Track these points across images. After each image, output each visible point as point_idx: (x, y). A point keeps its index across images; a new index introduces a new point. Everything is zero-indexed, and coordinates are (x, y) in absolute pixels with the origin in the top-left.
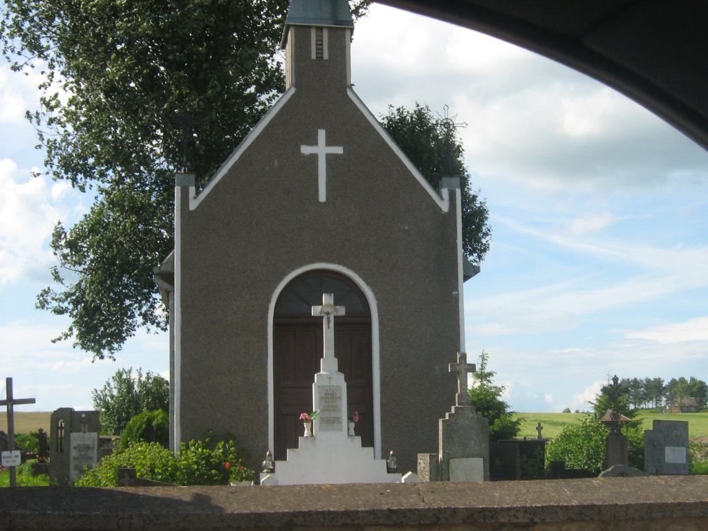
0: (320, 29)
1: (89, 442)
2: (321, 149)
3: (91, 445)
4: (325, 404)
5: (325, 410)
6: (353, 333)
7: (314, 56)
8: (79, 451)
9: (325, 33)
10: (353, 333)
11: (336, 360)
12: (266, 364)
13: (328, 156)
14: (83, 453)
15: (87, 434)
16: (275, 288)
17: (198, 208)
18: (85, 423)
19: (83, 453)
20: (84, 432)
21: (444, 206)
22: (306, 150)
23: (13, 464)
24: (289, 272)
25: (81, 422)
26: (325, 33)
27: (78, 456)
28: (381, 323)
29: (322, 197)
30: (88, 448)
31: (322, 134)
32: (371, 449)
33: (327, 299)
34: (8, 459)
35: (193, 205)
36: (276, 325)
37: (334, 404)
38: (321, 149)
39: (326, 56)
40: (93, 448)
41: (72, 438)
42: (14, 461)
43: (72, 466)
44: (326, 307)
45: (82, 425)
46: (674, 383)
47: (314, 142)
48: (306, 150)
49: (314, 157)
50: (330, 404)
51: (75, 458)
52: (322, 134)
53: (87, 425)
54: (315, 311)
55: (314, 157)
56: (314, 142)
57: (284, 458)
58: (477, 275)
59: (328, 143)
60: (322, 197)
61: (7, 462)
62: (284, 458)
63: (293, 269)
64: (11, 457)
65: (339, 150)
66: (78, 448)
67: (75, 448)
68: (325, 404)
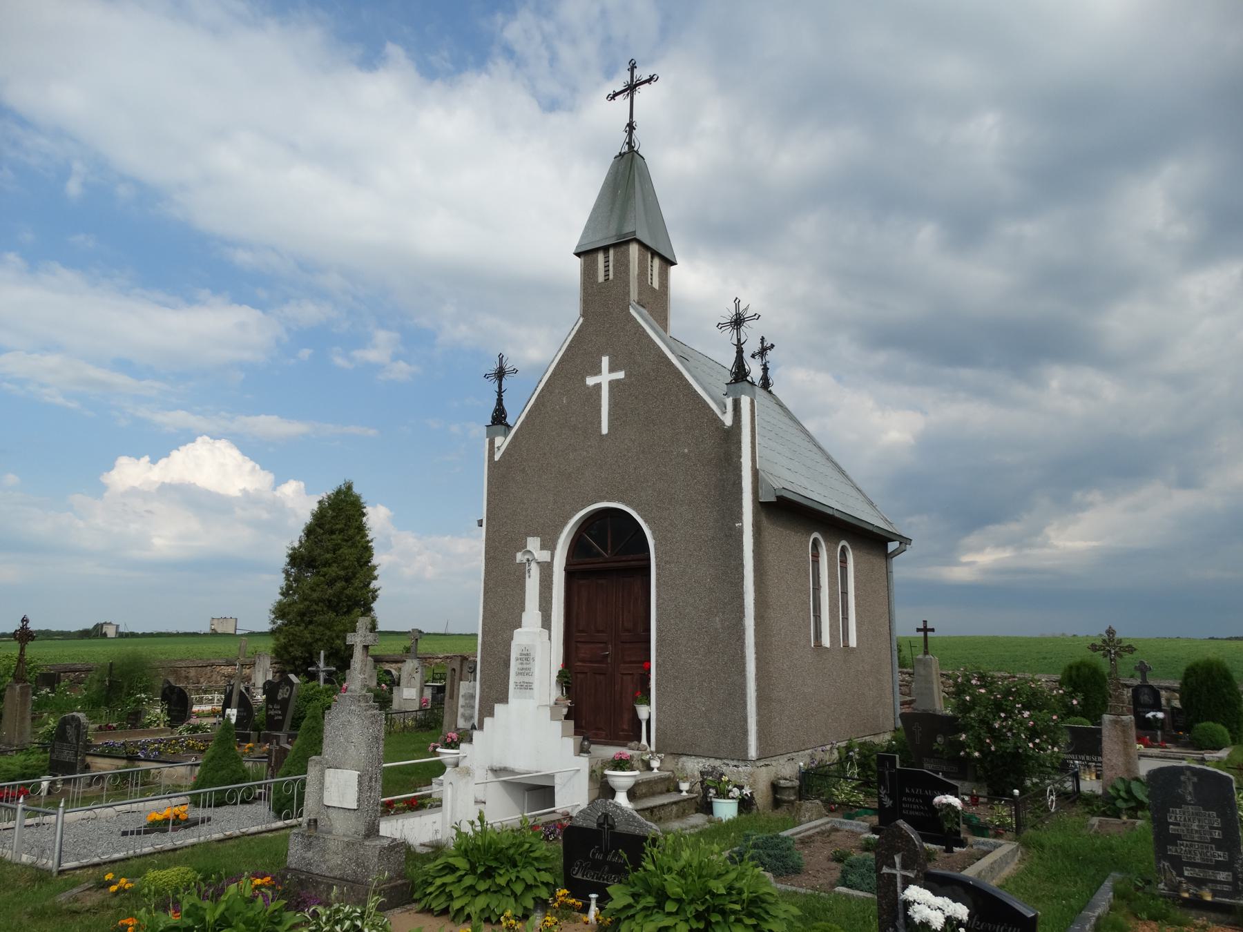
0: (605, 249)
2: (605, 378)
21: (728, 420)
29: (605, 430)
35: (497, 458)
60: (605, 430)
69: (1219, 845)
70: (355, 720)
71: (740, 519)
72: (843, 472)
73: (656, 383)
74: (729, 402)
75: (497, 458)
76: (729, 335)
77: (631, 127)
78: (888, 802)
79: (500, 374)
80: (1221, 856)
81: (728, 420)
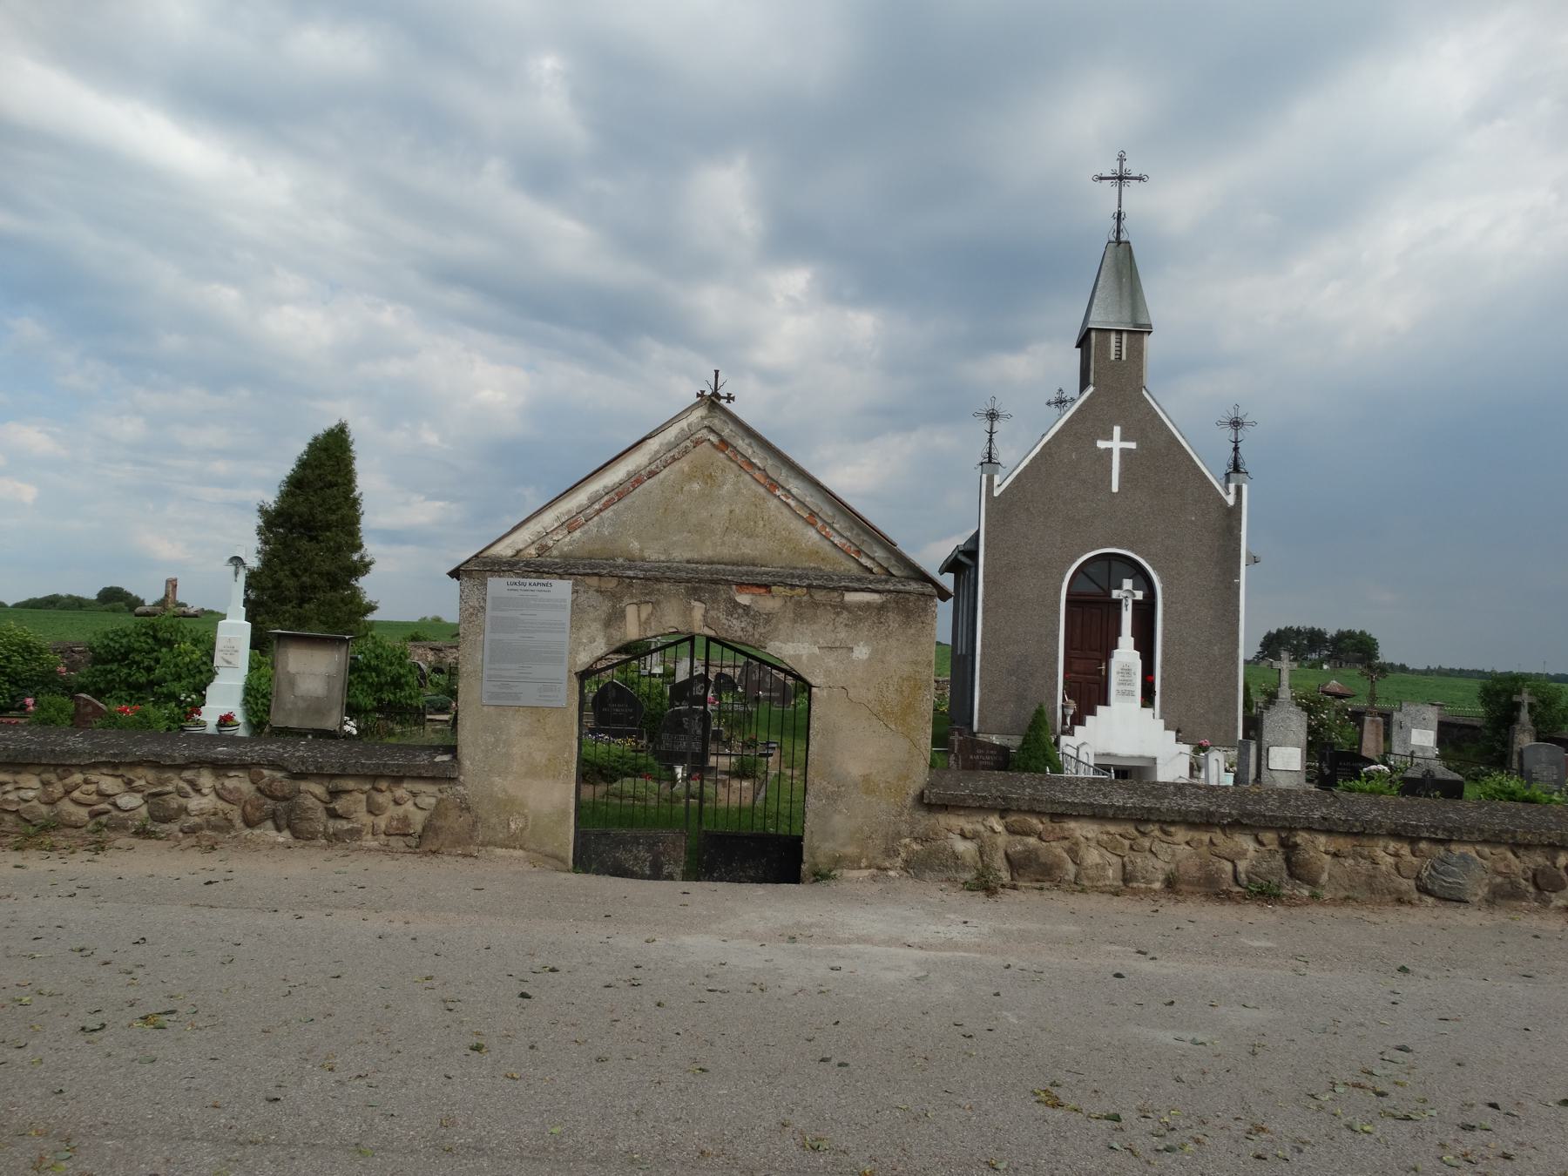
0: (1120, 332)
2: (1116, 444)
6: (1145, 612)
7: (1113, 357)
10: (1145, 612)
12: (1163, 679)
13: (1122, 450)
21: (1231, 500)
26: (1125, 336)
28: (1165, 605)
29: (1115, 489)
31: (1117, 430)
32: (1150, 711)
33: (1128, 584)
35: (996, 494)
36: (1068, 601)
38: (1116, 444)
44: (1127, 592)
46: (1342, 636)
49: (1109, 451)
52: (1117, 430)
54: (1115, 594)
55: (1109, 451)
57: (1082, 723)
59: (1111, 438)
60: (1115, 489)
62: (1082, 723)
69: (1556, 782)
70: (1294, 717)
71: (1238, 576)
72: (644, 440)
73: (1160, 454)
74: (1232, 487)
75: (996, 494)
76: (1229, 433)
77: (1119, 217)
78: (1327, 771)
79: (993, 416)
80: (1556, 787)
81: (1231, 500)
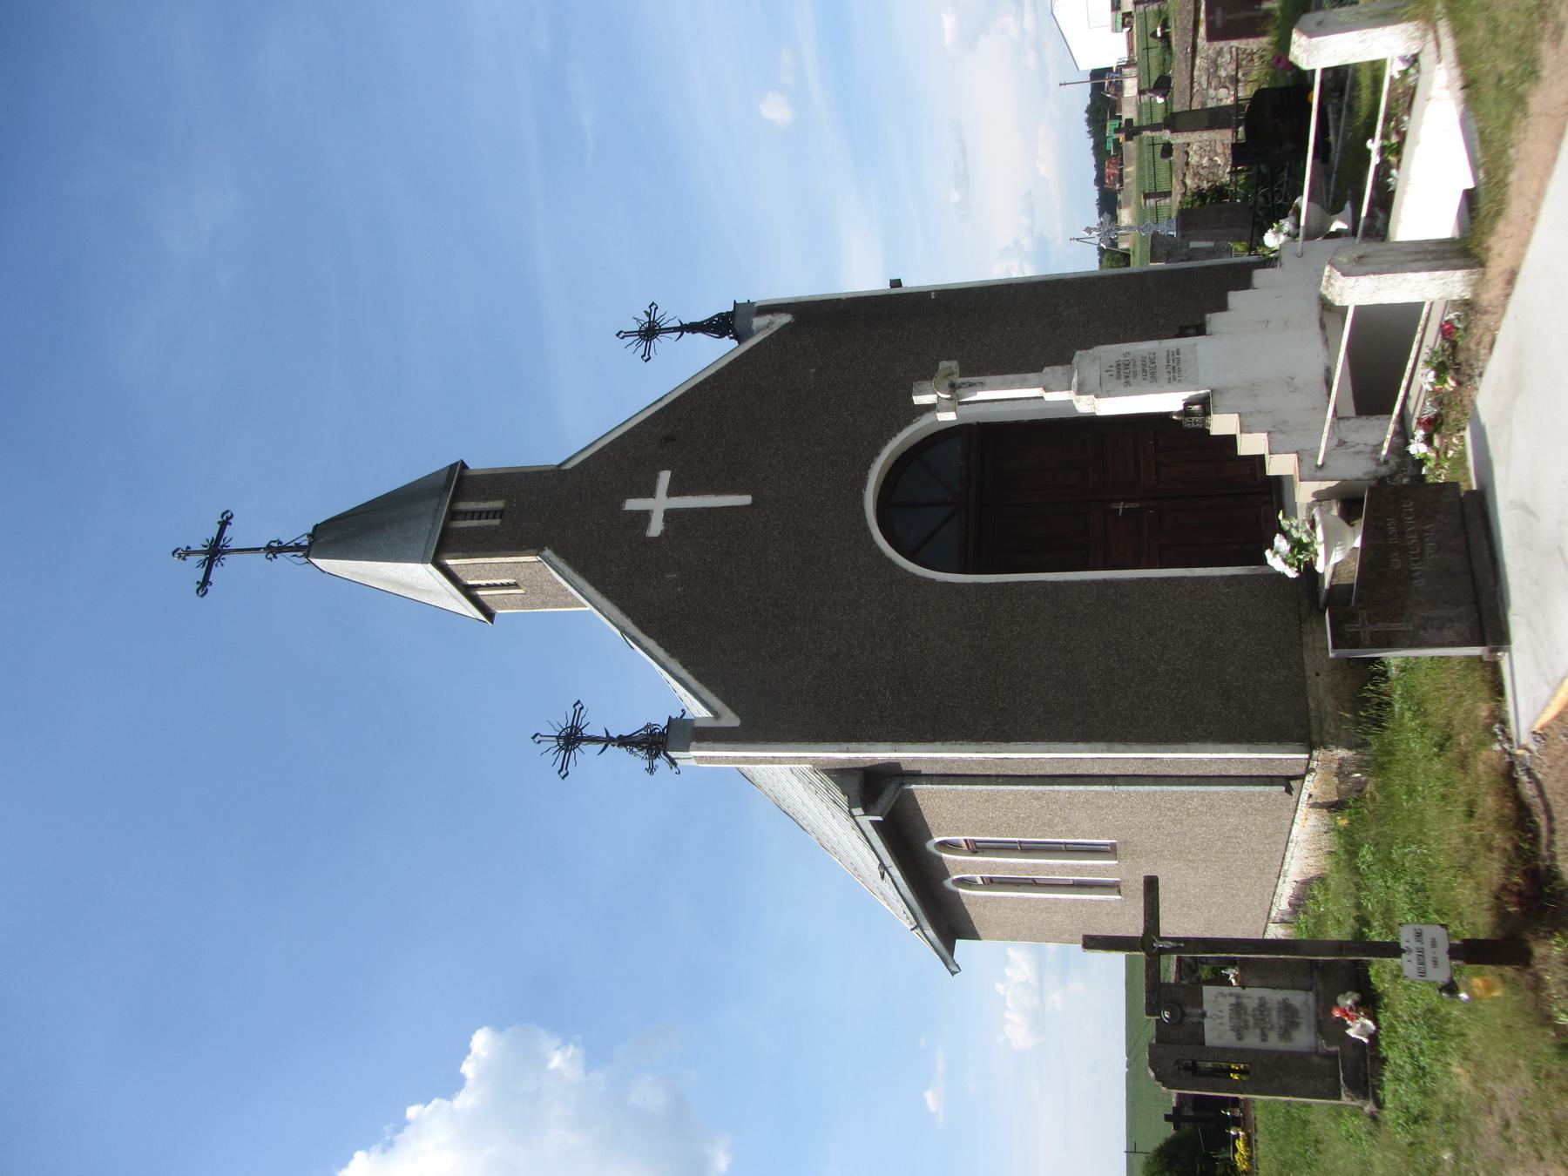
0: (453, 515)
1: (1226, 1005)
3: (1233, 1000)
4: (1140, 377)
5: (1153, 373)
7: (497, 522)
8: (1247, 1027)
9: (464, 506)
11: (1046, 369)
14: (1251, 1020)
15: (1206, 1007)
16: (906, 571)
17: (735, 711)
18: (1184, 1014)
19: (1251, 1020)
20: (1204, 1015)
22: (656, 528)
23: (1443, 946)
24: (878, 548)
25: (1181, 1021)
26: (464, 506)
27: (1258, 1032)
29: (746, 500)
30: (1238, 1008)
31: (633, 504)
34: (1429, 964)
37: (1139, 363)
38: (657, 505)
39: (498, 504)
40: (1238, 997)
41: (1217, 1043)
42: (1434, 944)
43: (1283, 1046)
45: (1187, 1020)
47: (645, 516)
48: (656, 528)
50: (1139, 369)
51: (1264, 1038)
53: (1188, 1010)
56: (645, 516)
58: (1122, 1145)
60: (746, 500)
61: (1435, 963)
63: (872, 542)
64: (1421, 953)
65: (665, 477)
66: (1239, 1031)
67: (1240, 1038)
68: (1140, 377)
